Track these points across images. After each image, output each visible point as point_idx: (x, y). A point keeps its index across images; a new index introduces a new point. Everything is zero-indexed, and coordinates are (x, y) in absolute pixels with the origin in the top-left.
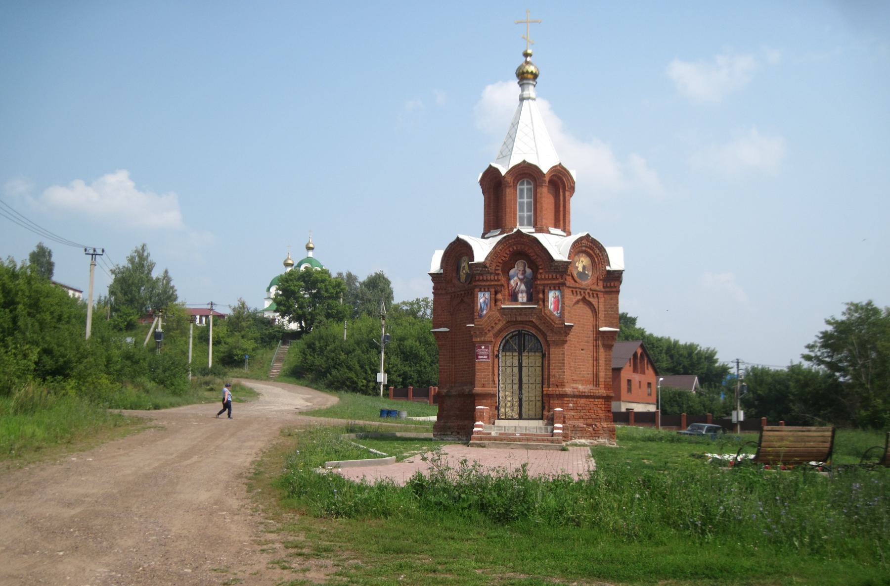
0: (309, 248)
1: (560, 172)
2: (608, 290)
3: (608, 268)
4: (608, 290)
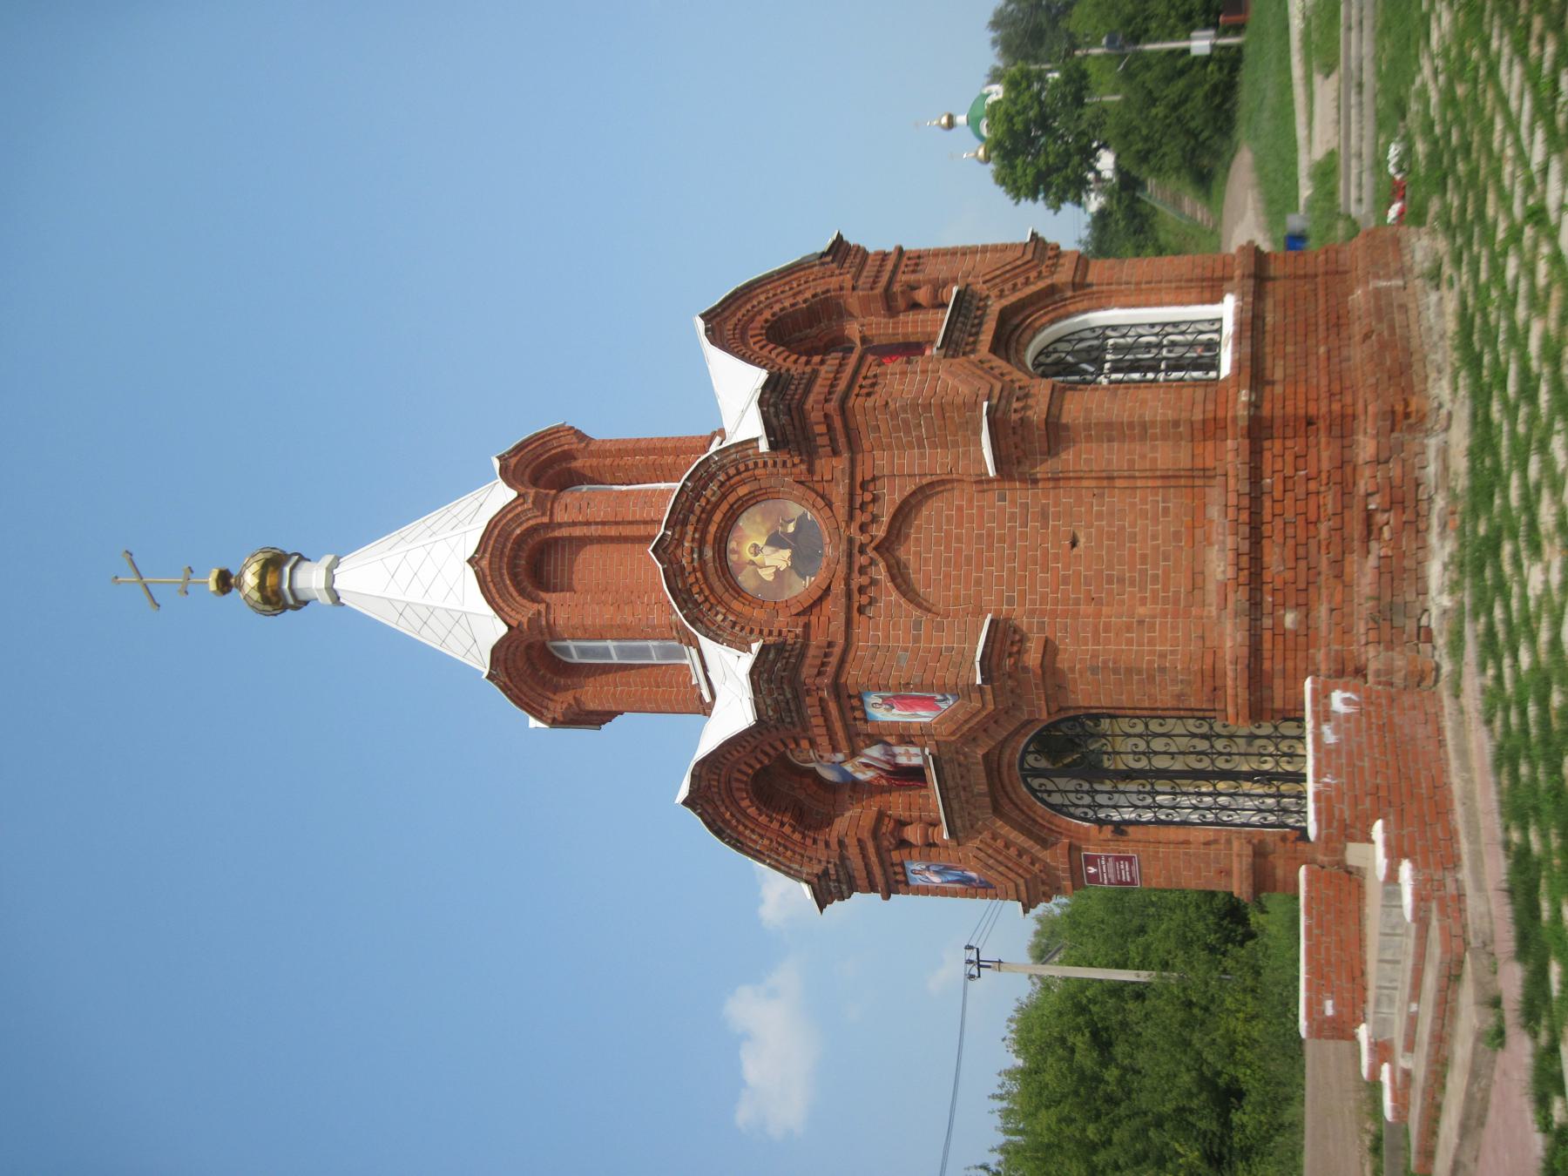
0: (951, 124)
1: (498, 554)
2: (842, 441)
3: (764, 446)
4: (842, 441)
